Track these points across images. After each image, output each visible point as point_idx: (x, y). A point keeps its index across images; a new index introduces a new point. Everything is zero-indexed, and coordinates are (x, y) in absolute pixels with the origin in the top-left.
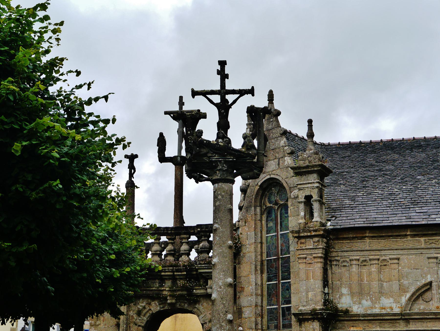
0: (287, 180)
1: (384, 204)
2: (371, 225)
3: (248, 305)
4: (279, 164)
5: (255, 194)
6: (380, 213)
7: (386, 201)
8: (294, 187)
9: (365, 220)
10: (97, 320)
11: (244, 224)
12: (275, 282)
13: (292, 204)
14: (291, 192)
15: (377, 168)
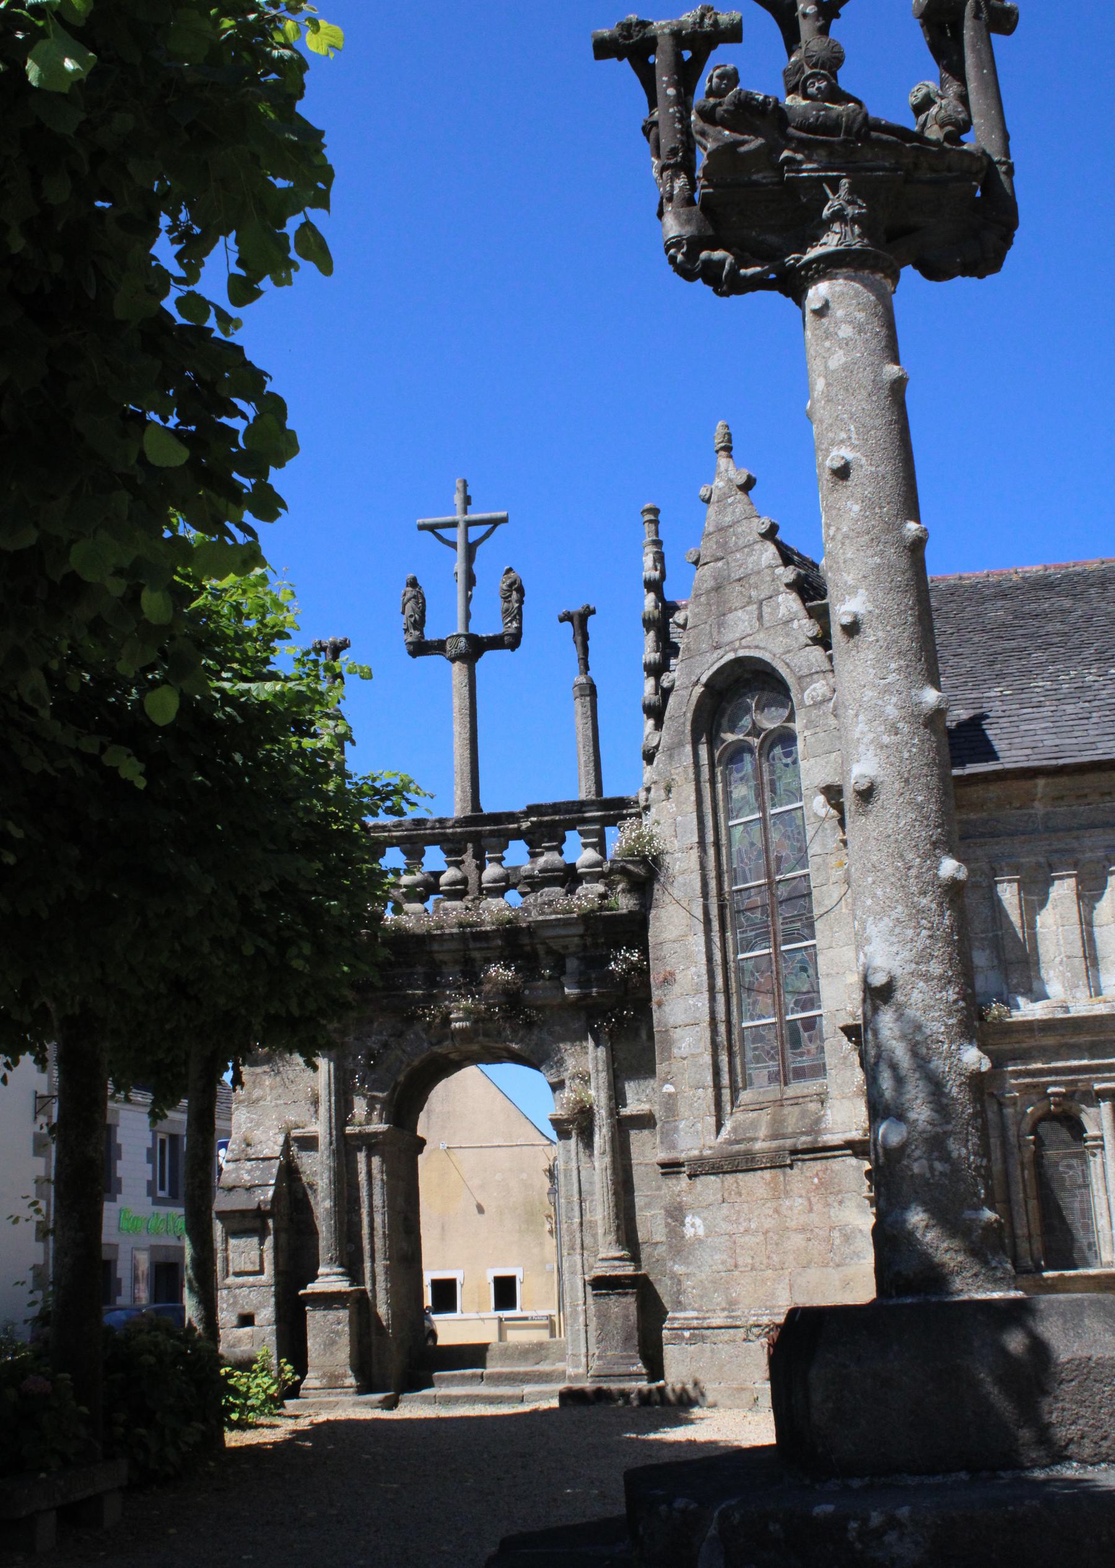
0: (788, 657)
1: (1069, 712)
2: (1054, 762)
3: (688, 1021)
4: (760, 617)
5: (692, 708)
6: (1065, 735)
7: (1072, 706)
9: (1029, 751)
10: (255, 1087)
12: (766, 951)
13: (809, 721)
14: (803, 690)
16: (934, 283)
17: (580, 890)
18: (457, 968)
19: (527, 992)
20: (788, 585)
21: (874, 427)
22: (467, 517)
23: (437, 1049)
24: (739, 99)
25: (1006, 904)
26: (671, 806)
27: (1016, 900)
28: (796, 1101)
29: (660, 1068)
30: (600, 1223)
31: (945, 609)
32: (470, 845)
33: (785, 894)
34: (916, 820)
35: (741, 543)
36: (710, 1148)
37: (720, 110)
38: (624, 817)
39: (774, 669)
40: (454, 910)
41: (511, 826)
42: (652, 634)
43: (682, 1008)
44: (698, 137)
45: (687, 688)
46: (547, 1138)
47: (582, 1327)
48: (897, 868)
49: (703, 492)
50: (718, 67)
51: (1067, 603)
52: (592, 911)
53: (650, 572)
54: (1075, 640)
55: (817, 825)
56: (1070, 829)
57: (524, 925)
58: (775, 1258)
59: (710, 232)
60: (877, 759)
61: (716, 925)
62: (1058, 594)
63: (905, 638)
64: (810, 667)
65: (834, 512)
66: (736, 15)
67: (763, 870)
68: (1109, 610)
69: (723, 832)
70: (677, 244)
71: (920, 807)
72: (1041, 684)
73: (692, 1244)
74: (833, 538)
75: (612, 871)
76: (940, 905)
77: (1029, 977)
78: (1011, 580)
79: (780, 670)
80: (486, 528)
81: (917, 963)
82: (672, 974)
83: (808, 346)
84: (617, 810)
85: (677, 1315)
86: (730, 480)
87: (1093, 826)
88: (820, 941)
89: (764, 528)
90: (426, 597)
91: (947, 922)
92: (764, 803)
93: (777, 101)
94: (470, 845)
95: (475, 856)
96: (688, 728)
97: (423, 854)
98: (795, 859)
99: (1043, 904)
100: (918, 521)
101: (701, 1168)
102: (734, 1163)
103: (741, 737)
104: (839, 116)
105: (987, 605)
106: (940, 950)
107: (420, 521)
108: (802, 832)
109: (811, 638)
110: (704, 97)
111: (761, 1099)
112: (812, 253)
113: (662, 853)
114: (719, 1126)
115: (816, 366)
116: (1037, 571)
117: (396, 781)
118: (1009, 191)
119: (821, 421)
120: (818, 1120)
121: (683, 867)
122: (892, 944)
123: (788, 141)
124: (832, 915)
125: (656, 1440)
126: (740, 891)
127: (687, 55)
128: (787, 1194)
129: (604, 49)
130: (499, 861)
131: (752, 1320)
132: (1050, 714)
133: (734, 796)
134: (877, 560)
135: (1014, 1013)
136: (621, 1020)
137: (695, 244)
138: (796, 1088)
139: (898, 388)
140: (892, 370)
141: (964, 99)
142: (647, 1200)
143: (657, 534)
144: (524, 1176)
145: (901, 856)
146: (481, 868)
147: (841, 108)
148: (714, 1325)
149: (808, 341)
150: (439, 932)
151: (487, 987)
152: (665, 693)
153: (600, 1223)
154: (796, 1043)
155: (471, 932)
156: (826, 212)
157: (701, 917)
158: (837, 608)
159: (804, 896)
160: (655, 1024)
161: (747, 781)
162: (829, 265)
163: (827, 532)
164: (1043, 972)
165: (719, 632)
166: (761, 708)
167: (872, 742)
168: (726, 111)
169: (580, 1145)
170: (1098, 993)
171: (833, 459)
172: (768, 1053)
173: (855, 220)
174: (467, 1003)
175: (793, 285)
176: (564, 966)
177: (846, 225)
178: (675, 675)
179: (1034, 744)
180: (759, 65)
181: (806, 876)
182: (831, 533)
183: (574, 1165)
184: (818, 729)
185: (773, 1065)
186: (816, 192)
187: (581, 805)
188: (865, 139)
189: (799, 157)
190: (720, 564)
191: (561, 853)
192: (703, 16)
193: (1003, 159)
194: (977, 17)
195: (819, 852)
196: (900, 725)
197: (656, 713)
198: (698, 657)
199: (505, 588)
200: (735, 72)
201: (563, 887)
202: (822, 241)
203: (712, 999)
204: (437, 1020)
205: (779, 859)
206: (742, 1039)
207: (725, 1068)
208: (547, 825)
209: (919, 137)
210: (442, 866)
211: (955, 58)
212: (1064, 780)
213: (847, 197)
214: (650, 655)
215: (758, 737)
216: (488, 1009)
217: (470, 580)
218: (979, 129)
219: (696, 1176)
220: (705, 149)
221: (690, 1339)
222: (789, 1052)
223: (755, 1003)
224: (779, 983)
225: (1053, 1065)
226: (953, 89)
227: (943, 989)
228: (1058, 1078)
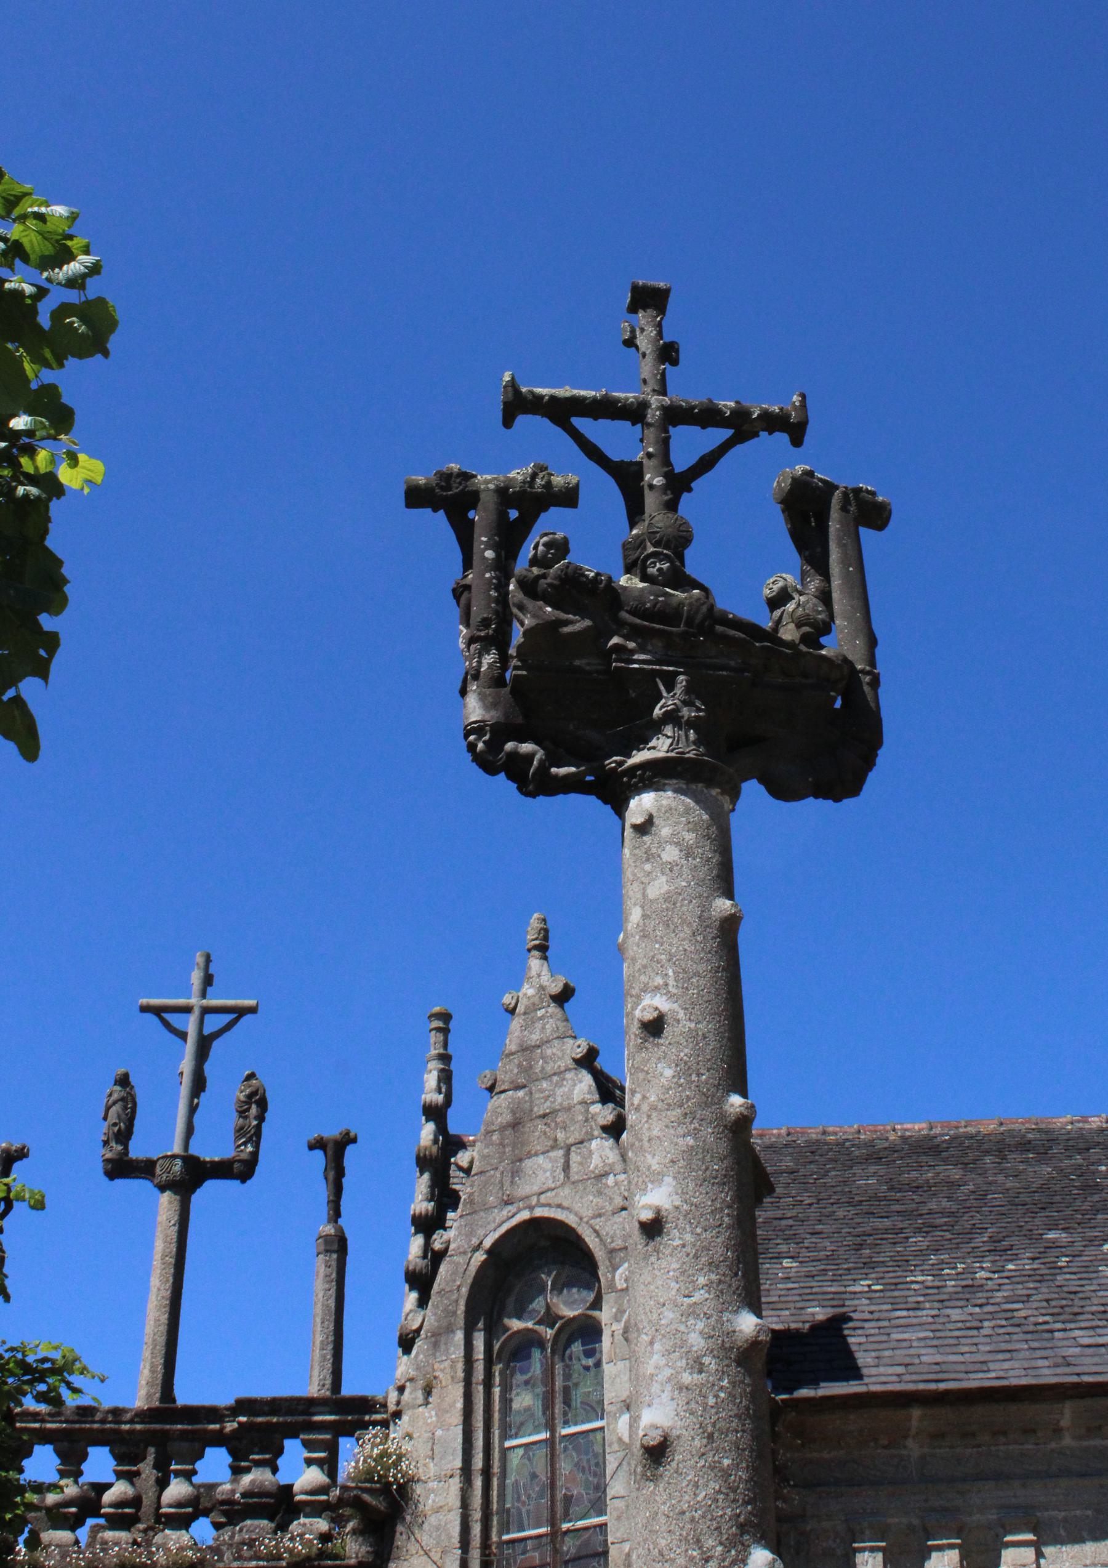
0: (598, 1223)
1: (954, 1318)
2: (933, 1386)
4: (566, 1168)
5: (469, 1281)
6: (948, 1349)
9: (900, 1370)
14: (615, 1268)
15: (897, 1207)
17: (295, 1527)
20: (604, 1129)
21: (697, 974)
22: (204, 1002)
24: (566, 574)
26: (428, 1414)
31: (802, 1172)
32: (151, 1450)
33: (573, 1551)
34: (719, 1492)
38: (365, 1426)
39: (579, 1238)
40: (116, 1544)
41: (212, 1427)
42: (426, 1176)
44: (515, 610)
45: (465, 1253)
48: (692, 1558)
49: (507, 999)
50: (546, 535)
51: (956, 1173)
52: (308, 1558)
53: (432, 1096)
54: (965, 1223)
55: (621, 1454)
59: (520, 720)
60: (674, 1403)
62: (946, 1161)
63: (719, 1245)
65: (641, 1076)
66: (573, 479)
67: (545, 1514)
68: (1009, 1185)
70: (478, 729)
71: (726, 1474)
72: (920, 1278)
74: (638, 1109)
78: (887, 1139)
79: (587, 1239)
80: (228, 1018)
83: (626, 866)
84: (358, 1414)
86: (542, 988)
89: (579, 1053)
90: (137, 1100)
92: (553, 1418)
94: (151, 1450)
95: (157, 1466)
96: (462, 1307)
97: (84, 1457)
98: (590, 1501)
100: (744, 1094)
104: (681, 604)
105: (857, 1170)
107: (144, 1001)
108: (601, 1464)
110: (527, 566)
112: (639, 757)
113: (412, 1479)
115: (632, 892)
116: (920, 1130)
117: (57, 1356)
118: (873, 705)
119: (634, 960)
121: (439, 1502)
123: (619, 627)
126: (512, 1542)
127: (514, 514)
129: (416, 497)
130: (188, 1475)
132: (930, 1320)
133: (515, 1406)
134: (690, 1141)
137: (500, 732)
139: (729, 927)
140: (723, 906)
141: (825, 597)
143: (445, 1045)
145: (698, 1541)
146: (163, 1484)
147: (684, 595)
149: (625, 861)
152: (436, 1258)
156: (657, 712)
158: (637, 1198)
161: (534, 1386)
162: (655, 775)
163: (631, 1099)
166: (558, 1288)
167: (669, 1380)
171: (644, 1010)
173: (691, 724)
175: (615, 792)
177: (680, 729)
178: (451, 1234)
179: (907, 1360)
180: (594, 537)
181: (603, 1526)
182: (636, 1101)
187: (309, 1405)
189: (631, 645)
190: (521, 1093)
192: (534, 476)
193: (868, 668)
194: (844, 509)
195: (622, 1493)
196: (706, 1360)
197: (421, 1282)
198: (482, 1214)
200: (565, 541)
201: (271, 1520)
202: (651, 745)
205: (568, 1500)
208: (260, 1429)
209: (772, 636)
210: (108, 1477)
213: (683, 697)
214: (421, 1205)
215: (552, 1327)
217: (199, 1084)
218: (842, 632)
220: (522, 624)
226: (814, 584)
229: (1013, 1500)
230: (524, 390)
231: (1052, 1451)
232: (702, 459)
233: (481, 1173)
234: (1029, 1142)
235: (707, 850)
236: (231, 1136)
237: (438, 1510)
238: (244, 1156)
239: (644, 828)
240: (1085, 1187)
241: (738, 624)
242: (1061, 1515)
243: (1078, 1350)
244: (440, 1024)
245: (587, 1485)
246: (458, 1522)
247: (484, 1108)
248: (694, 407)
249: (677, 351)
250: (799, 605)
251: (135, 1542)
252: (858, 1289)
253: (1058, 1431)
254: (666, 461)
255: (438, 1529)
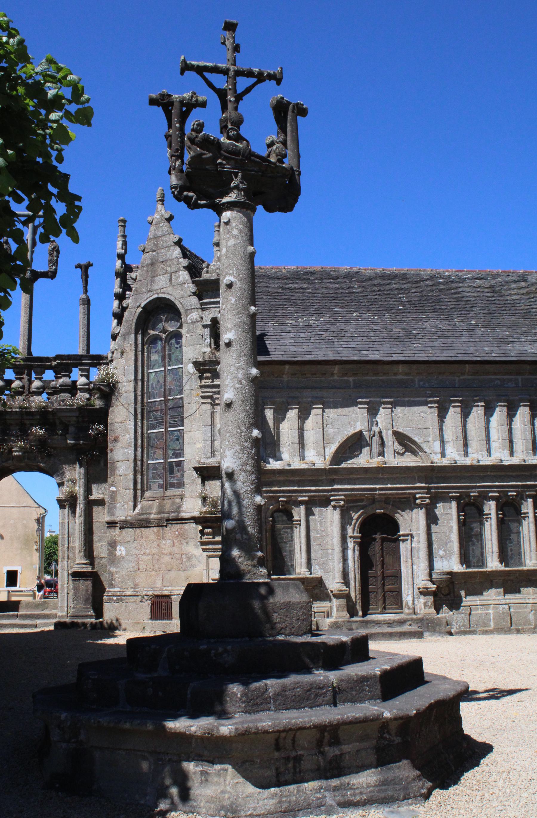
1: (301, 336)
2: (293, 359)
3: (124, 459)
4: (171, 280)
5: (136, 317)
6: (299, 347)
7: (303, 334)
8: (191, 309)
9: (283, 353)
11: (120, 356)
12: (161, 430)
14: (187, 316)
16: (268, 213)
18: (17, 427)
19: (49, 441)
20: (184, 267)
23: (5, 464)
25: (268, 418)
26: (123, 361)
27: (272, 417)
28: (170, 498)
29: (110, 479)
30: (77, 547)
33: (172, 405)
35: (164, 245)
36: (130, 516)
37: (197, 139)
38: (101, 364)
39: (175, 305)
41: (48, 363)
42: (119, 279)
43: (122, 453)
45: (134, 308)
46: (38, 504)
47: (66, 594)
48: (238, 432)
49: (149, 219)
50: (197, 121)
51: (305, 285)
52: (83, 406)
54: (307, 303)
56: (297, 388)
57: (51, 410)
58: (156, 566)
59: (188, 184)
61: (139, 417)
62: (302, 281)
64: (191, 306)
65: (225, 300)
66: (205, 98)
68: (323, 291)
69: (146, 375)
70: (176, 188)
72: (291, 322)
73: (120, 559)
74: (224, 309)
75: (94, 389)
76: (251, 446)
77: (275, 450)
78: (282, 272)
81: (242, 466)
82: (118, 437)
84: (98, 360)
85: (111, 590)
86: (162, 215)
87: (307, 387)
88: (186, 428)
89: (176, 240)
91: (253, 452)
93: (218, 140)
99: (283, 419)
101: (125, 525)
102: (141, 523)
103: (157, 333)
104: (240, 149)
105: (271, 282)
106: (250, 462)
109: (193, 293)
111: (154, 496)
113: (117, 382)
114: (135, 507)
118: (298, 182)
120: (180, 507)
121: (126, 389)
122: (234, 459)
124: (192, 417)
125: (102, 643)
126: (151, 402)
128: (164, 538)
129: (153, 102)
131: (145, 593)
133: (152, 359)
134: (239, 320)
135: (268, 465)
136: (92, 456)
137: (182, 188)
138: (170, 492)
140: (251, 249)
142: (99, 538)
143: (124, 232)
144: (25, 522)
148: (127, 594)
150: (10, 410)
151: (31, 437)
152: (124, 309)
153: (77, 547)
154: (172, 471)
155: (25, 411)
156: (232, 185)
157: (133, 413)
159: (180, 407)
160: (109, 460)
162: (231, 206)
164: (281, 449)
165: (151, 284)
166: (167, 321)
167: (232, 386)
168: (199, 141)
169: (70, 512)
170: (303, 459)
171: (227, 280)
172: (159, 475)
173: (242, 190)
174: (21, 444)
175: (219, 210)
176: (68, 430)
178: (130, 301)
180: (209, 120)
183: (66, 520)
184: (192, 334)
185: (161, 481)
186: (229, 177)
187: (81, 357)
188: (249, 159)
189: (224, 162)
190: (154, 253)
191: (70, 377)
192: (192, 97)
194: (293, 112)
196: (243, 381)
197: (119, 317)
199: (50, 249)
200: (203, 123)
202: (229, 195)
203: (136, 450)
204: (6, 451)
205: (170, 389)
206: (148, 469)
207: (139, 481)
208: (64, 364)
211: (284, 125)
212: (297, 367)
214: (118, 290)
216: (31, 447)
219: (123, 528)
221: (116, 600)
222: (168, 476)
223: (155, 453)
224: (166, 445)
225: (282, 488)
227: (250, 475)
228: (284, 494)
229: (317, 395)
230: (188, 62)
231: (330, 380)
232: (247, 89)
233: (140, 280)
234: (331, 275)
235: (246, 230)
236: (47, 262)
237: (126, 392)
238: (52, 270)
239: (227, 223)
240: (349, 293)
241: (258, 156)
242: (331, 400)
243: (341, 349)
244: (123, 224)
245: (177, 385)
246: (133, 395)
247: (141, 258)
248: (245, 71)
249: (239, 48)
250: (277, 148)
251: (24, 400)
252: (269, 325)
253: (333, 374)
254: (235, 91)
255: (126, 398)
